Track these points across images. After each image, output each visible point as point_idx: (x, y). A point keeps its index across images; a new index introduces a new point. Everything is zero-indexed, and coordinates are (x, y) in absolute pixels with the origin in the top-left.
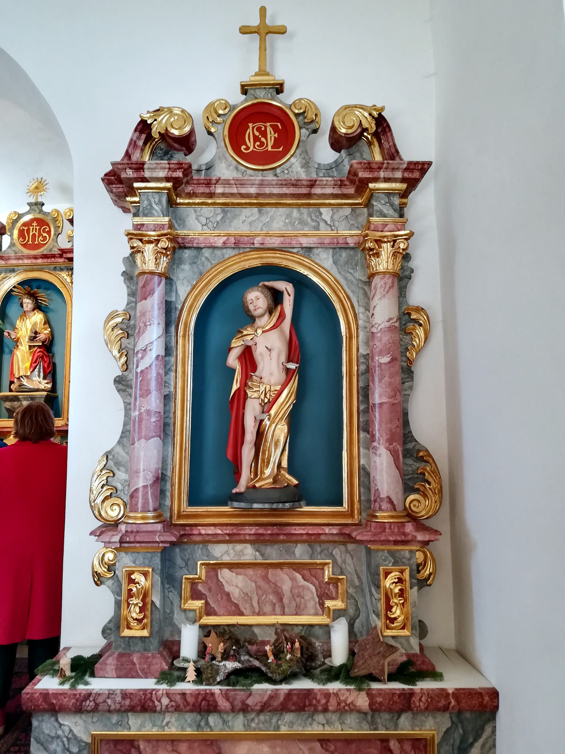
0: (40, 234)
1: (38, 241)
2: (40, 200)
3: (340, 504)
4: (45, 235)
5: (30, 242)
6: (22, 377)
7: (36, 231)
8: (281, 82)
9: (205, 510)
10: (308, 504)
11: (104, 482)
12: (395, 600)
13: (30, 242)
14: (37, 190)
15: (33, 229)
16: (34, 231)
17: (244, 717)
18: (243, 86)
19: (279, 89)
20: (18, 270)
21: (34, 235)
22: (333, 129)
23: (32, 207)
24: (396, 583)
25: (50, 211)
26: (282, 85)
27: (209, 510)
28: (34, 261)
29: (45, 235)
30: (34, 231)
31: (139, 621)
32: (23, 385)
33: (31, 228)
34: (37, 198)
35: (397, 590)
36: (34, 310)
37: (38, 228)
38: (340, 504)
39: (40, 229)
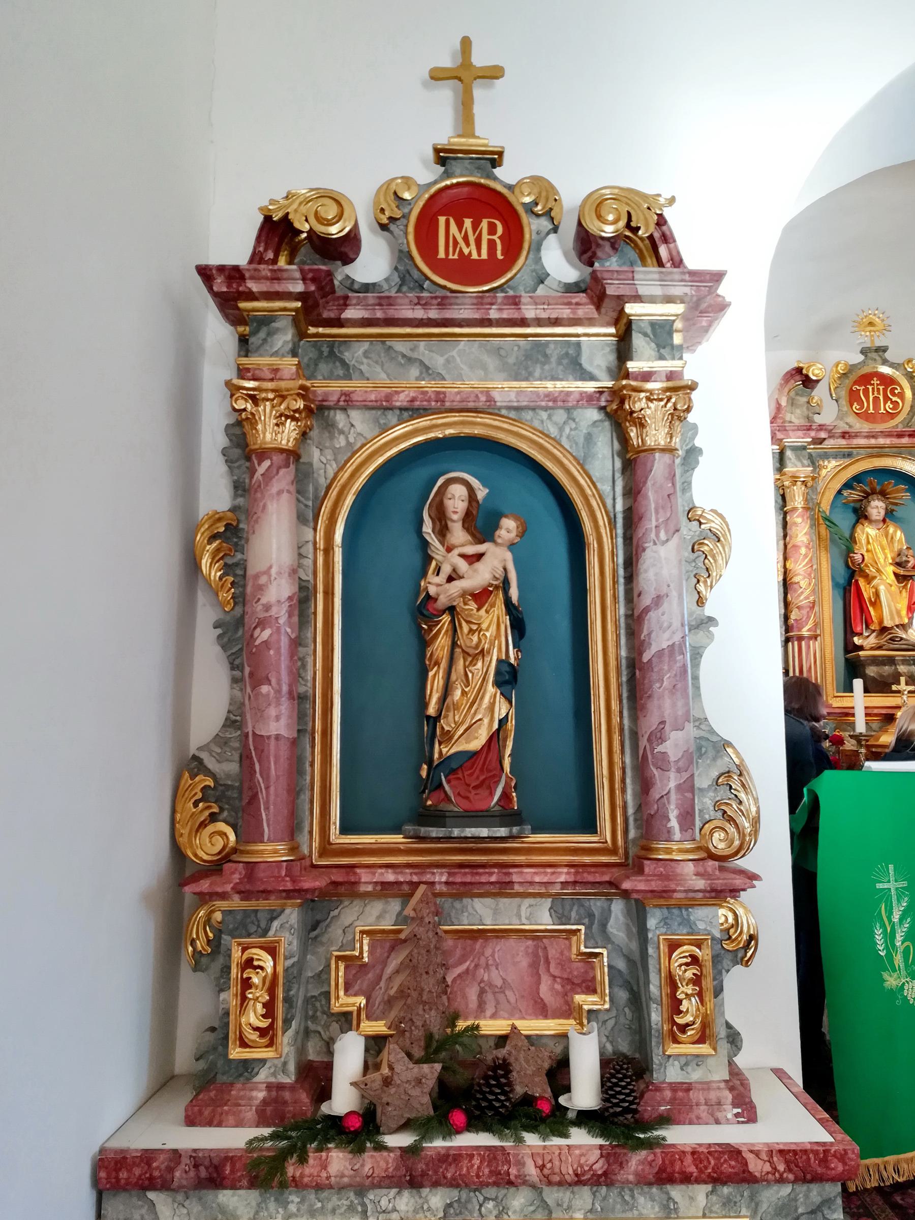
0: (886, 399)
1: (885, 409)
2: (878, 343)
3: (345, 829)
4: (894, 399)
5: (871, 411)
6: (897, 626)
7: (879, 393)
8: (499, 149)
9: (373, 841)
10: (535, 831)
11: (199, 796)
12: (685, 989)
13: (871, 411)
14: (872, 328)
15: (873, 389)
16: (876, 393)
17: (316, 1194)
18: (437, 151)
19: (495, 159)
20: (858, 454)
21: (876, 399)
22: (288, 214)
23: (869, 354)
24: (687, 964)
25: (901, 362)
26: (501, 154)
27: (379, 841)
28: (895, 441)
29: (894, 399)
30: (876, 393)
31: (262, 1032)
32: (902, 639)
33: (870, 388)
34: (872, 341)
35: (689, 974)
36: (884, 521)
37: (881, 388)
38: (345, 829)
39: (885, 391)
